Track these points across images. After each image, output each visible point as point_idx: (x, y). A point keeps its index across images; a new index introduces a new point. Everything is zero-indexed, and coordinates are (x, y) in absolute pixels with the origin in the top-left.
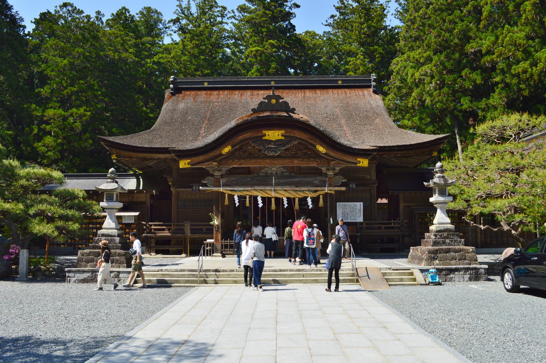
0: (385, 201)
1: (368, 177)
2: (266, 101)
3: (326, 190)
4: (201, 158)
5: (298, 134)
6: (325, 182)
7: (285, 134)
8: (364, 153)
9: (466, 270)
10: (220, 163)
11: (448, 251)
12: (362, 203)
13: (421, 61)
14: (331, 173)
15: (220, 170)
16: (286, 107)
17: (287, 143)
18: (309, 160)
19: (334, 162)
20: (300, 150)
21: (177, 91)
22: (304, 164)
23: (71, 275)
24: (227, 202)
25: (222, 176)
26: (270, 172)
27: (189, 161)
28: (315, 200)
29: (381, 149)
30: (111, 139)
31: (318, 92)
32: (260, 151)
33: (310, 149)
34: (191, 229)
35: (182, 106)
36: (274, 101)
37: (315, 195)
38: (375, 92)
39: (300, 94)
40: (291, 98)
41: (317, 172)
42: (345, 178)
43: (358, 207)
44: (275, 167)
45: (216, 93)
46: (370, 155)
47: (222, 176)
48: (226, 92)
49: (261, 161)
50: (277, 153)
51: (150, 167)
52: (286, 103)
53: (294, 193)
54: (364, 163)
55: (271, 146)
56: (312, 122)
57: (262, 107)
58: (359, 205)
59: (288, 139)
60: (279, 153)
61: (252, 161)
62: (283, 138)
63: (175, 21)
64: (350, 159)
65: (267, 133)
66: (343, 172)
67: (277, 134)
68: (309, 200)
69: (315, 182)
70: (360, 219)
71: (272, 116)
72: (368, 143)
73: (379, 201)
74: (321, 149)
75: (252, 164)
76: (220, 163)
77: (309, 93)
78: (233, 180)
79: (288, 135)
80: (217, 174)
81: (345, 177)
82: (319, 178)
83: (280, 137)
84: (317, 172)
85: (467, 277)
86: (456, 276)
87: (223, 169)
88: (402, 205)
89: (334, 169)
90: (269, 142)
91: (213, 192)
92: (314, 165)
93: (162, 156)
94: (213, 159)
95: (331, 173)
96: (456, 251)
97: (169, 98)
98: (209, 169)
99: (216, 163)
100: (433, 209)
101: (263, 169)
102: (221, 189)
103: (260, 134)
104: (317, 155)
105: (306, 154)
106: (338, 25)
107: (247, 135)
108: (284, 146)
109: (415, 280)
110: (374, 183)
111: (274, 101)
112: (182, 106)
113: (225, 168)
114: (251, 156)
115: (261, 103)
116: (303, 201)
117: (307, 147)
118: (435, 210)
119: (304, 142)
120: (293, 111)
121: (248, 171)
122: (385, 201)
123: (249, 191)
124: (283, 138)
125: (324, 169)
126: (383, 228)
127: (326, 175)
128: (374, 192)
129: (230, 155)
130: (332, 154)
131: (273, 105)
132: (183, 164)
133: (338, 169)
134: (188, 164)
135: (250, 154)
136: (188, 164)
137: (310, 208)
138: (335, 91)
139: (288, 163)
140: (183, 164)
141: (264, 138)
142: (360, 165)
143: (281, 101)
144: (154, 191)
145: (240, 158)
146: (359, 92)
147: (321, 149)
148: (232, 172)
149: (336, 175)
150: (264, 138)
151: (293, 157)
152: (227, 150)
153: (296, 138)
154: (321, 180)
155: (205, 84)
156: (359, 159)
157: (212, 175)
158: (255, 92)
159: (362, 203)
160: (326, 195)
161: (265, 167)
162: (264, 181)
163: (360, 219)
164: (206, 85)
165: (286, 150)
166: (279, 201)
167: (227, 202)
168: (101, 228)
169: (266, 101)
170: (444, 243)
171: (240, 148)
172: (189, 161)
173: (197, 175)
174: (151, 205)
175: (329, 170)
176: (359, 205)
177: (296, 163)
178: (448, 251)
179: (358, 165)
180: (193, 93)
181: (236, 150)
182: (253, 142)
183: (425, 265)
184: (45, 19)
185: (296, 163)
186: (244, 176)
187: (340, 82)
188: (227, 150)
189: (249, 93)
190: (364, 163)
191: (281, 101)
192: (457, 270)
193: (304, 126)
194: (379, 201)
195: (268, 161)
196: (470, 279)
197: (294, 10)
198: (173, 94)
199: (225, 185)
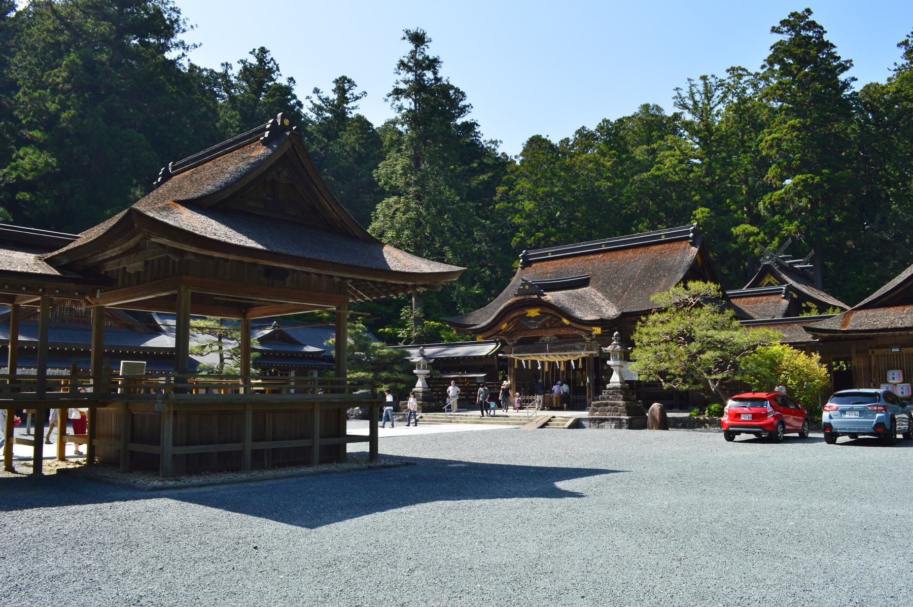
5: (549, 311)
9: (613, 420)
11: (606, 405)
13: (539, 224)
24: (516, 366)
25: (514, 345)
28: (576, 362)
37: (576, 358)
39: (738, 300)
47: (514, 345)
68: (572, 363)
74: (566, 321)
83: (538, 314)
85: (613, 425)
86: (606, 424)
90: (530, 318)
96: (612, 405)
100: (610, 372)
102: (512, 356)
104: (563, 326)
118: (612, 371)
123: (532, 357)
127: (584, 341)
130: (574, 325)
147: (566, 321)
148: (521, 342)
153: (548, 314)
160: (584, 359)
162: (541, 350)
167: (516, 366)
170: (608, 398)
178: (606, 405)
192: (606, 420)
196: (616, 427)
199: (515, 352)
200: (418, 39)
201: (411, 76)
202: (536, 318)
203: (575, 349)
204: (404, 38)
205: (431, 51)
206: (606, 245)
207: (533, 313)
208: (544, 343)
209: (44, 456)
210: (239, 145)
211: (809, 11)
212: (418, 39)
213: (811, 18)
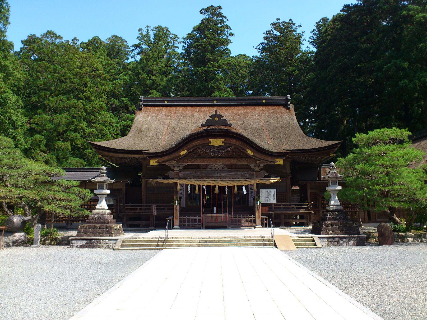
0: (297, 188)
1: (284, 171)
2: (211, 118)
4: (165, 158)
5: (233, 141)
6: (253, 175)
7: (225, 142)
8: (279, 155)
10: (178, 161)
12: (275, 190)
14: (257, 169)
15: (178, 167)
16: (225, 123)
17: (226, 148)
18: (242, 159)
19: (259, 161)
20: (236, 152)
23: (74, 242)
25: (180, 171)
26: (214, 168)
27: (157, 160)
29: (293, 152)
30: (93, 142)
32: (207, 153)
33: (242, 152)
34: (157, 209)
36: (217, 119)
40: (229, 115)
41: (248, 168)
42: (267, 172)
43: (273, 193)
44: (217, 165)
46: (284, 156)
47: (180, 171)
49: (208, 160)
50: (219, 154)
51: (126, 163)
52: (225, 120)
53: (232, 183)
54: (281, 162)
55: (215, 150)
57: (208, 123)
60: (220, 155)
61: (202, 160)
62: (223, 144)
63: (137, 46)
64: (270, 159)
65: (212, 141)
67: (219, 142)
69: (246, 175)
70: (275, 202)
71: (216, 129)
72: (284, 146)
73: (294, 188)
74: (250, 152)
76: (178, 161)
78: (188, 174)
79: (227, 142)
80: (176, 169)
81: (267, 172)
82: (250, 172)
83: (221, 144)
84: (248, 168)
87: (180, 165)
88: (309, 192)
89: (259, 166)
92: (245, 163)
93: (136, 156)
94: (173, 159)
95: (257, 169)
98: (170, 166)
99: (176, 162)
101: (209, 165)
103: (207, 142)
104: (248, 156)
105: (239, 155)
106: (264, 50)
107: (198, 142)
108: (225, 150)
109: (315, 245)
110: (289, 176)
111: (217, 119)
113: (182, 166)
114: (200, 156)
115: (208, 120)
117: (240, 150)
119: (238, 147)
120: (230, 125)
121: (198, 167)
122: (297, 188)
124: (223, 144)
125: (252, 166)
126: (295, 208)
127: (254, 170)
128: (289, 181)
129: (186, 156)
130: (258, 155)
131: (216, 121)
132: (153, 162)
133: (262, 166)
134: (156, 162)
135: (200, 155)
136: (156, 162)
139: (226, 161)
140: (153, 162)
141: (210, 144)
142: (278, 163)
143: (221, 118)
144: (129, 181)
145: (192, 158)
147: (250, 152)
149: (261, 170)
150: (210, 144)
151: (231, 157)
152: (183, 152)
153: (232, 145)
154: (250, 174)
155: (165, 102)
156: (276, 159)
157: (173, 170)
159: (275, 190)
161: (211, 164)
162: (210, 175)
163: (275, 202)
164: (166, 102)
165: (225, 153)
168: (95, 209)
169: (211, 118)
171: (193, 151)
172: (157, 160)
173: (162, 171)
174: (126, 191)
175: (255, 166)
179: (276, 163)
180: (157, 108)
181: (190, 152)
182: (202, 147)
183: (176, 184)
184: (30, 42)
186: (195, 170)
187: (264, 102)
188: (183, 152)
190: (281, 162)
191: (221, 118)
194: (294, 188)
195: (212, 160)
197: (230, 38)
207: (217, 142)
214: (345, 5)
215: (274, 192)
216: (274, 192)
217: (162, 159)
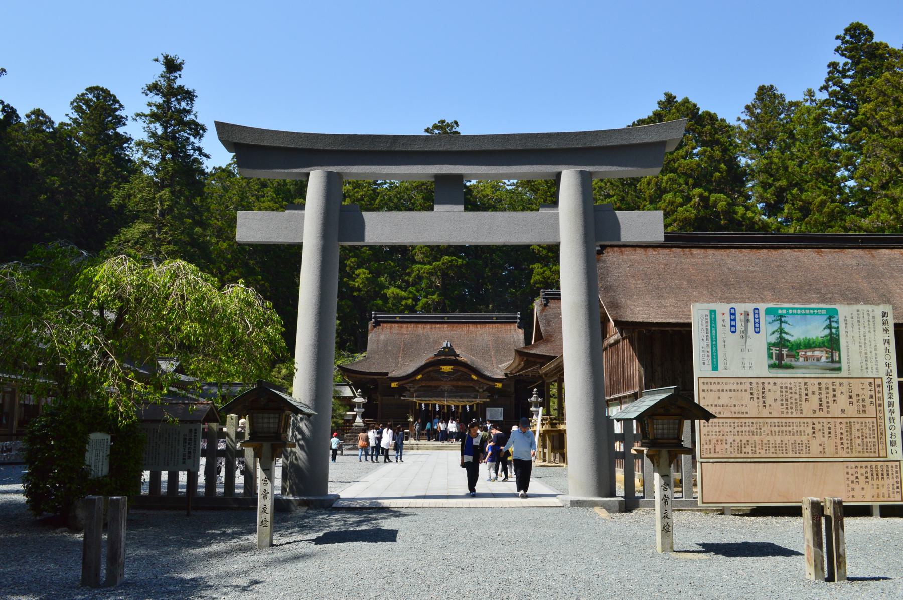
3: (478, 401)
5: (461, 369)
21: (377, 324)
22: (465, 384)
31: (478, 326)
35: (382, 337)
38: (519, 327)
41: (473, 389)
45: (405, 325)
47: (416, 391)
48: (413, 325)
56: (469, 363)
58: (501, 410)
59: (455, 371)
64: (491, 383)
66: (487, 390)
70: (501, 419)
74: (474, 377)
75: (433, 384)
77: (472, 327)
84: (473, 389)
90: (444, 373)
91: (409, 401)
97: (372, 330)
104: (473, 380)
107: (431, 369)
112: (382, 337)
113: (417, 387)
116: (464, 407)
120: (458, 356)
127: (478, 391)
130: (481, 380)
132: (394, 385)
137: (21, 498)
138: (491, 326)
139: (455, 383)
140: (394, 385)
146: (508, 327)
147: (474, 377)
151: (459, 380)
152: (419, 377)
153: (458, 371)
158: (434, 326)
162: (441, 395)
163: (501, 419)
166: (449, 407)
173: (401, 390)
176: (501, 410)
177: (460, 384)
185: (460, 384)
188: (419, 377)
189: (429, 326)
193: (464, 365)
198: (375, 327)
200: (172, 66)
201: (159, 100)
202: (449, 373)
203: (468, 397)
204: (156, 60)
205: (184, 80)
206: (449, 318)
207: (447, 369)
208: (444, 392)
209: (329, 479)
210: (401, 254)
211: (456, 123)
212: (172, 66)
213: (457, 129)
214: (670, 99)
215: (626, 236)
216: (626, 236)
217: (401, 383)
